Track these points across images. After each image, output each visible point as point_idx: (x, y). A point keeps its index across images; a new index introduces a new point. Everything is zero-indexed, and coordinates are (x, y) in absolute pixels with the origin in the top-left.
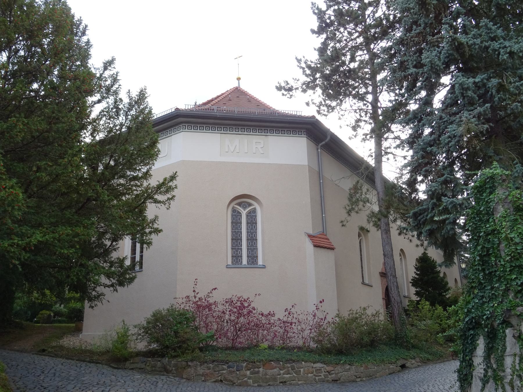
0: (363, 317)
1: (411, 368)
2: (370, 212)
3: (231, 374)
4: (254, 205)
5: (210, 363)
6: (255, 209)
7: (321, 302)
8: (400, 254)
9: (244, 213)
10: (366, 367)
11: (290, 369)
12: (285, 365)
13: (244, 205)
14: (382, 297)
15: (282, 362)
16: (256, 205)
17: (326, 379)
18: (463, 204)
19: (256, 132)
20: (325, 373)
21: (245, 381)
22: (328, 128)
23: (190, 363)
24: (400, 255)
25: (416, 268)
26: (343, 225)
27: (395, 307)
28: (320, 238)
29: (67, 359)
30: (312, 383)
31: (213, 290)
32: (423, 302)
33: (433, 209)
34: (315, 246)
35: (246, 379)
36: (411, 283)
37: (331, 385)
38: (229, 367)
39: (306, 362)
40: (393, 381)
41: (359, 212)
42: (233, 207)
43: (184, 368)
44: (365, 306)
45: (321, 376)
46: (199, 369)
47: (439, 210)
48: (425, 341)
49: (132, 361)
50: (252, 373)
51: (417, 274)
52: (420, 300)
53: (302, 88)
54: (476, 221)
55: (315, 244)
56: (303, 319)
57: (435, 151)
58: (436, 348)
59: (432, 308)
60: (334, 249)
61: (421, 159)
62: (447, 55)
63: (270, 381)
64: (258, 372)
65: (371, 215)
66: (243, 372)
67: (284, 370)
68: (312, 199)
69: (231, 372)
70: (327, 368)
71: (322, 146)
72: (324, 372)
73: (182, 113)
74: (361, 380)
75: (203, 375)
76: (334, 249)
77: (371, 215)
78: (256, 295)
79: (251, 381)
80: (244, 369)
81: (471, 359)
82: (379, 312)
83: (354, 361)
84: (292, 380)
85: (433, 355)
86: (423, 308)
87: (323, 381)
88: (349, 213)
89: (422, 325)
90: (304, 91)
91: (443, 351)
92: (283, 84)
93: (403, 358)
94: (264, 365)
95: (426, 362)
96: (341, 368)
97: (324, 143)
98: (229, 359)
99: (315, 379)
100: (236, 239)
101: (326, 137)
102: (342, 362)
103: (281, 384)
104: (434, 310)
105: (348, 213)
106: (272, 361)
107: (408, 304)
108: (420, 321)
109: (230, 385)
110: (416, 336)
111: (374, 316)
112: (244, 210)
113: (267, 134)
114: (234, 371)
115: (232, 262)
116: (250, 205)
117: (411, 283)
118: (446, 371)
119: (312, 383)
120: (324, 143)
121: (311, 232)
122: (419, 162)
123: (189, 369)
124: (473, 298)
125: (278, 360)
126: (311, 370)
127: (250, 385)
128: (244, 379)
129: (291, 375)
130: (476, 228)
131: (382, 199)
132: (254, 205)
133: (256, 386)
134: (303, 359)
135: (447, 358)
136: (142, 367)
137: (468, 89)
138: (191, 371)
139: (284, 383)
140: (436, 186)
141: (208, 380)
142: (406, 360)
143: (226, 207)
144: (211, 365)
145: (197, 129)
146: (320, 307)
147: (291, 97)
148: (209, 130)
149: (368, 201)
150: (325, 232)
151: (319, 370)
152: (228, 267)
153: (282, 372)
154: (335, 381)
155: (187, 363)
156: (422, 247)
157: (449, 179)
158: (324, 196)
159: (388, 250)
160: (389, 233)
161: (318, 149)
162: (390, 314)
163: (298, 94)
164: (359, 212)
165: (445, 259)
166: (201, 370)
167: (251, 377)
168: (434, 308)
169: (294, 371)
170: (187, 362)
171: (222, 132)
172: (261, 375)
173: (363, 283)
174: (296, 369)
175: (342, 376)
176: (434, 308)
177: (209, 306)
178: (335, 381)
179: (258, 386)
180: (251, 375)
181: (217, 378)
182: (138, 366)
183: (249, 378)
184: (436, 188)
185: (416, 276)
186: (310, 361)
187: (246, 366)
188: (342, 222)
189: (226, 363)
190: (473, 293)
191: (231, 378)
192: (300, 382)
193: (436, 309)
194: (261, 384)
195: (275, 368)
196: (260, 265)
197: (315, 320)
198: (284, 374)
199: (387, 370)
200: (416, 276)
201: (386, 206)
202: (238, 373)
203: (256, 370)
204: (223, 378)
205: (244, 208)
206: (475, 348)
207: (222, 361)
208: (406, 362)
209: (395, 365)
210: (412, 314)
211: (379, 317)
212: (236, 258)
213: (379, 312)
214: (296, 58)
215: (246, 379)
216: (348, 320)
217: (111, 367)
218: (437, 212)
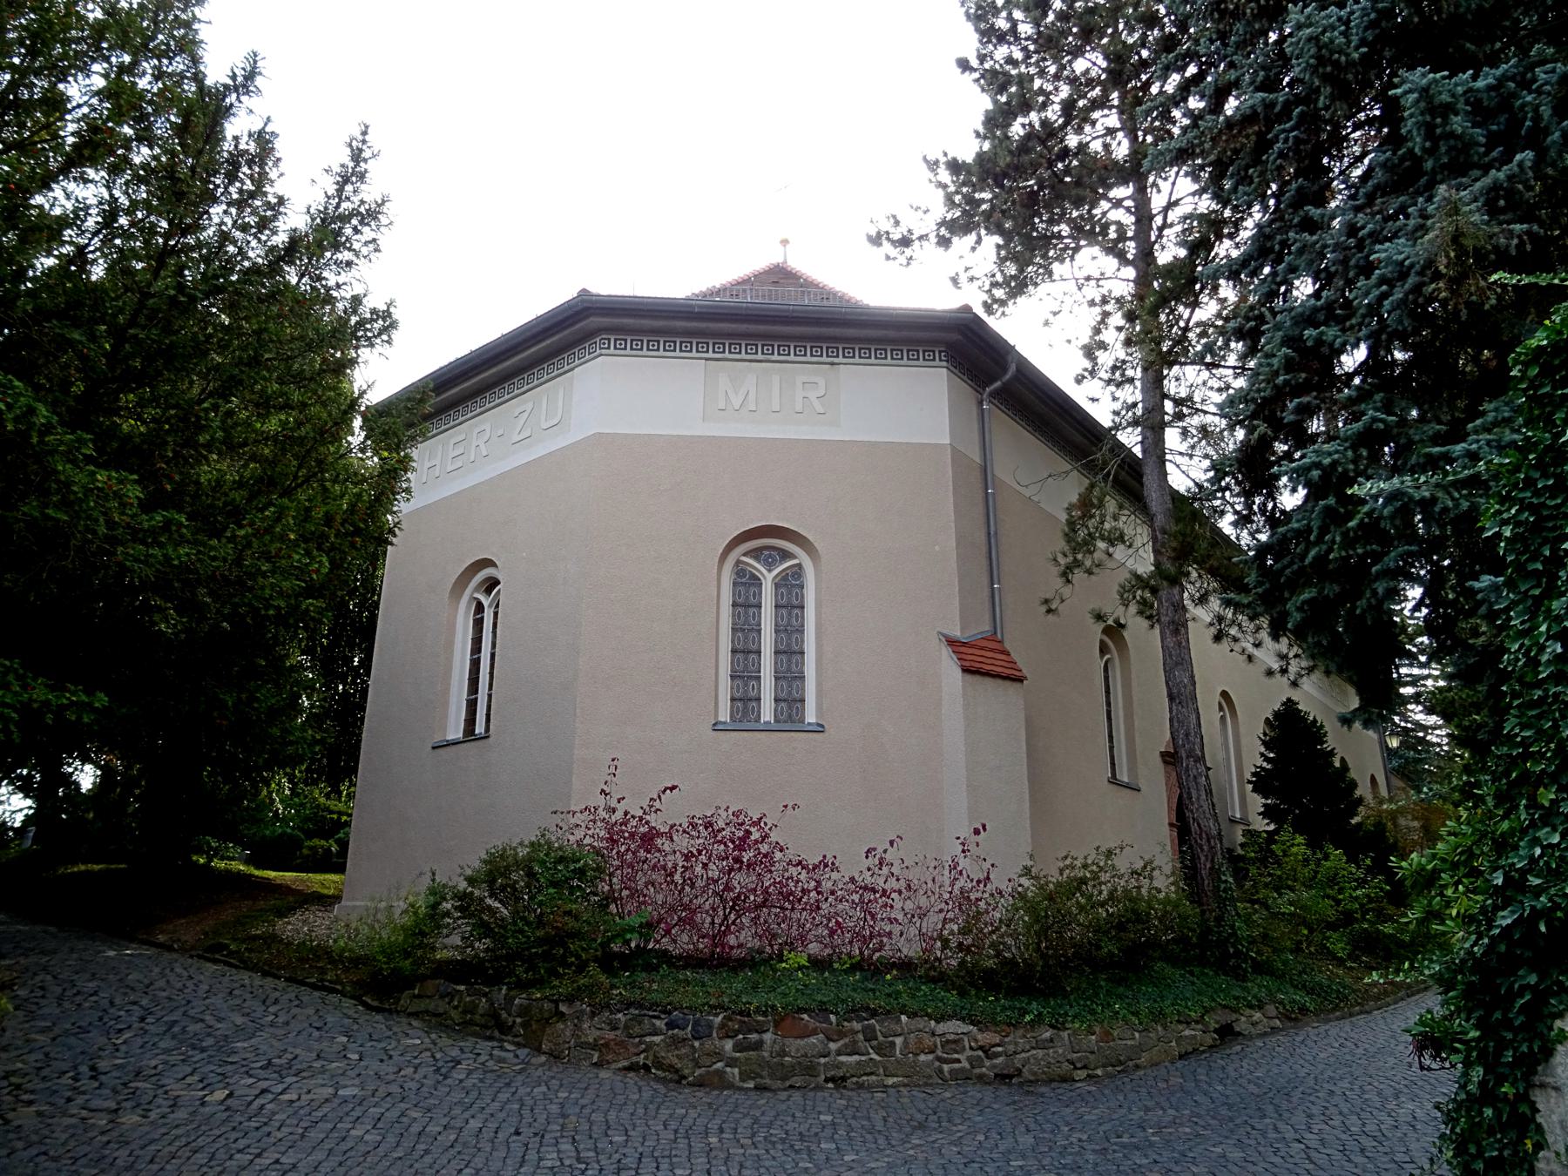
0: (1104, 877)
1: (1251, 1038)
2: (1128, 576)
5: (619, 1011)
6: (799, 566)
7: (977, 832)
8: (1220, 704)
9: (768, 578)
10: (1108, 1034)
11: (861, 1036)
12: (846, 1024)
13: (770, 556)
14: (1167, 821)
15: (836, 1014)
16: (802, 557)
17: (977, 1071)
18: (1433, 500)
19: (805, 355)
20: (971, 1053)
21: (717, 1071)
22: (1012, 343)
24: (1221, 708)
25: (1264, 743)
26: (1049, 611)
27: (1202, 850)
28: (982, 648)
29: (265, 974)
30: (931, 1085)
31: (664, 792)
32: (1284, 836)
33: (1324, 531)
34: (966, 670)
36: (1249, 782)
37: (988, 1093)
39: (912, 1015)
40: (1190, 1085)
41: (1095, 570)
42: (738, 562)
43: (547, 1020)
44: (1112, 845)
45: (958, 1061)
47: (1348, 530)
48: (1292, 952)
49: (416, 992)
50: (738, 1047)
51: (1267, 759)
52: (1276, 832)
53: (938, 235)
54: (1537, 493)
55: (967, 664)
56: (923, 880)
57: (1331, 338)
58: (1325, 974)
59: (1314, 853)
60: (1022, 681)
61: (1281, 372)
62: (1373, 16)
63: (795, 1075)
64: (758, 1045)
65: (1133, 583)
66: (714, 1042)
67: (841, 1042)
68: (960, 540)
69: (676, 1042)
70: (979, 1037)
71: (993, 395)
72: (971, 1048)
74: (1088, 1076)
75: (594, 1046)
76: (1022, 681)
77: (1133, 583)
78: (786, 806)
79: (736, 1071)
80: (715, 1035)
81: (1524, 1097)
82: (1151, 862)
83: (1066, 1014)
84: (866, 1074)
85: (1319, 995)
86: (1285, 854)
87: (962, 1077)
88: (1066, 575)
89: (1284, 904)
90: (944, 242)
91: (1348, 980)
92: (886, 226)
93: (1225, 1007)
94: (777, 1025)
95: (1294, 1017)
96: (1025, 1036)
97: (998, 384)
98: (676, 998)
99: (941, 1071)
100: (745, 652)
101: (1005, 370)
102: (1028, 1018)
103: (830, 1085)
104: (1319, 860)
105: (1064, 574)
106: (805, 1011)
107: (1241, 839)
108: (1277, 889)
109: (671, 1081)
110: (1265, 936)
111: (1140, 875)
112: (770, 571)
113: (836, 360)
114: (684, 1040)
115: (731, 717)
116: (786, 555)
117: (1249, 782)
118: (1360, 1051)
119: (931, 1085)
120: (998, 384)
121: (956, 633)
122: (1276, 386)
123: (561, 1026)
124: (1533, 824)
125: (823, 1010)
126: (928, 1041)
127: (731, 1086)
128: (715, 1067)
129: (863, 1058)
130: (1536, 528)
131: (1164, 532)
132: (795, 557)
133: (750, 1089)
134: (905, 1006)
135: (1359, 1004)
136: (441, 1010)
137: (1448, 110)
138: (564, 1029)
139: (839, 1081)
140: (1337, 452)
141: (608, 1063)
142: (1236, 1010)
143: (717, 560)
144: (620, 1015)
145: (641, 349)
146: (972, 847)
147: (908, 264)
148: (675, 350)
149: (1121, 538)
150: (999, 636)
151: (954, 1044)
152: (717, 727)
153: (833, 1046)
154: (1003, 1078)
155: (557, 1007)
156: (1285, 679)
157: (1381, 426)
158: (996, 533)
159: (1182, 681)
160: (1183, 631)
161: (981, 403)
162: (1190, 871)
163: (927, 252)
164: (1095, 570)
165: (1361, 700)
166: (592, 1031)
167: (737, 1059)
168: (1319, 856)
169: (874, 1043)
170: (556, 1002)
172: (766, 1054)
173: (1114, 780)
174: (881, 1038)
175: (1026, 1062)
176: (1319, 856)
177: (648, 839)
178: (1003, 1078)
179: (756, 1088)
181: (634, 1059)
182: (431, 1005)
183: (731, 1063)
184: (1336, 456)
185: (1265, 764)
186: (927, 1015)
187: (722, 1026)
188: (1046, 601)
189: (664, 1012)
190: (1533, 804)
192: (890, 1081)
193: (1326, 858)
194: (768, 1081)
195: (814, 1032)
196: (809, 724)
197: (958, 885)
198: (839, 1053)
199: (1173, 1044)
200: (1265, 764)
201: (1174, 550)
202: (697, 1044)
203: (754, 1036)
204: (651, 1058)
205: (770, 567)
206: (1548, 1052)
207: (653, 1005)
208: (1234, 1016)
209: (1200, 1026)
210: (1253, 871)
211: (1151, 878)
212: (745, 702)
213: (1151, 862)
214: (925, 158)
215: (719, 1065)
216: (1059, 884)
217: (365, 1004)
218: (1338, 539)
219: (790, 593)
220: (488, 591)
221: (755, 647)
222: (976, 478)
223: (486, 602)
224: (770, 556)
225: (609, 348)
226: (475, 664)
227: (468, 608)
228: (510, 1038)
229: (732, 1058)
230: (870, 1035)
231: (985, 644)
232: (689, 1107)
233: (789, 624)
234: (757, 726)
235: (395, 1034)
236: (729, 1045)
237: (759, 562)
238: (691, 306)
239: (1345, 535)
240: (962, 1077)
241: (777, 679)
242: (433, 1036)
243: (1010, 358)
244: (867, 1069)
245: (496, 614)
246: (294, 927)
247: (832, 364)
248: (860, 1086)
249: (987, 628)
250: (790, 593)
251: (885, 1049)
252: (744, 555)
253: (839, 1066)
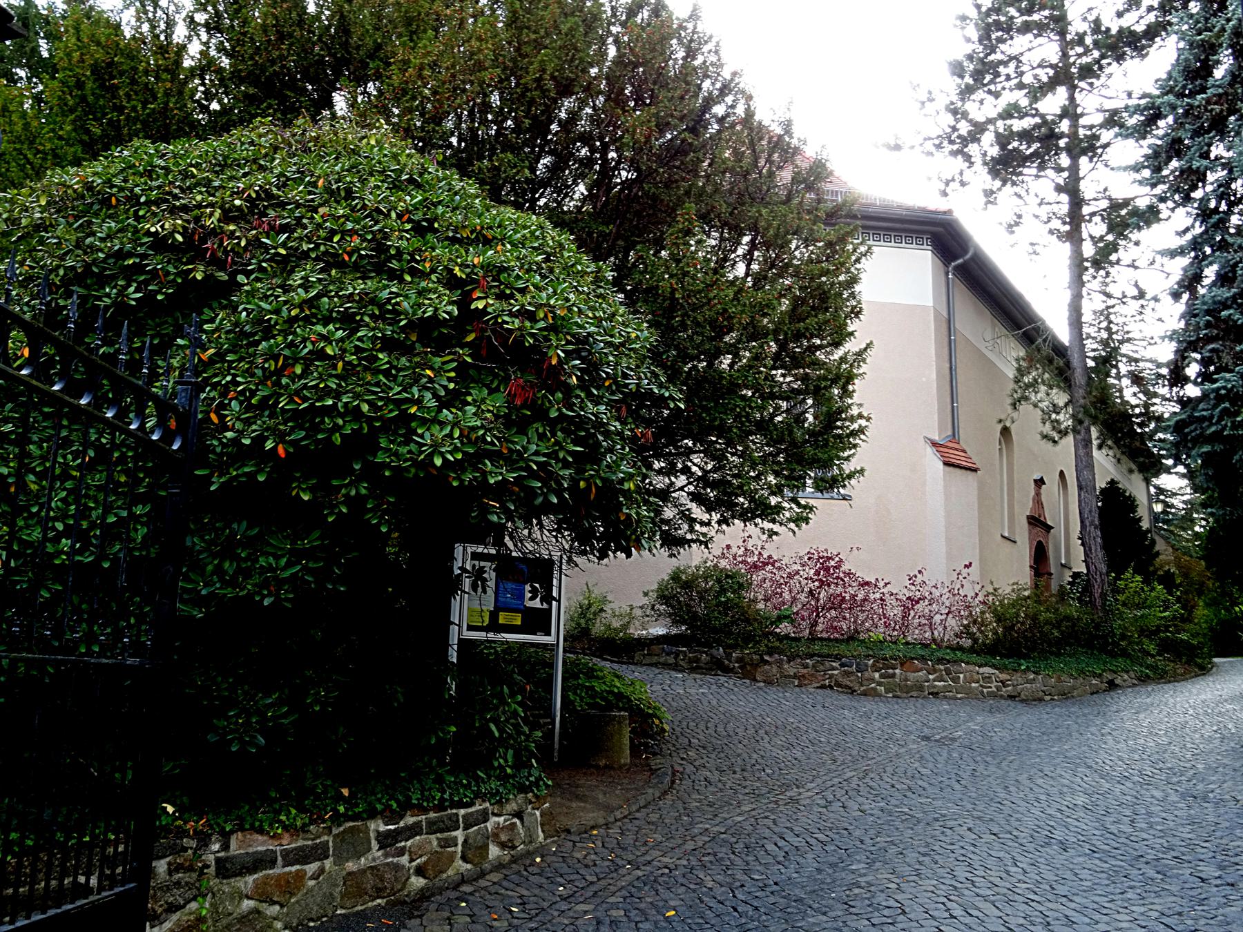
23: (767, 658)
33: (1220, 419)
34: (946, 464)
38: (842, 665)
39: (967, 663)
46: (786, 666)
50: (882, 676)
69: (847, 674)
75: (795, 677)
87: (993, 695)
88: (1014, 406)
94: (902, 665)
95: (1144, 680)
97: (960, 261)
101: (966, 252)
120: (960, 261)
121: (936, 438)
126: (976, 677)
127: (880, 696)
139: (935, 694)
142: (1115, 672)
151: (987, 679)
153: (931, 677)
161: (947, 274)
166: (790, 669)
178: (1011, 697)
183: (879, 684)
187: (873, 665)
195: (921, 670)
198: (934, 680)
222: (945, 326)
230: (948, 672)
232: (867, 705)
236: (877, 675)
239: (1233, 423)
240: (993, 695)
244: (947, 689)
248: (945, 697)
251: (956, 680)
253: (935, 687)
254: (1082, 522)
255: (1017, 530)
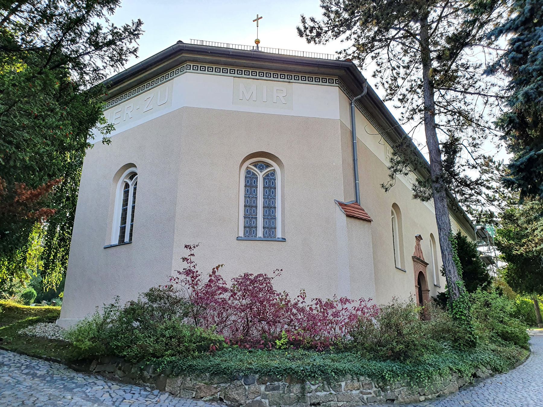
3: (237, 390)
4: (272, 166)
6: (274, 170)
9: (261, 175)
16: (275, 166)
28: (353, 207)
34: (348, 216)
35: (258, 398)
42: (248, 167)
71: (355, 100)
73: (186, 47)
79: (267, 401)
88: (392, 176)
112: (261, 172)
113: (291, 81)
115: (263, 235)
116: (268, 165)
120: (360, 96)
121: (342, 200)
132: (272, 166)
150: (358, 202)
152: (238, 239)
161: (351, 104)
171: (236, 75)
180: (267, 393)
183: (265, 397)
191: (236, 397)
196: (278, 238)
198: (316, 390)
205: (261, 169)
219: (270, 182)
220: (131, 178)
221: (254, 205)
223: (130, 183)
224: (261, 165)
225: (190, 69)
226: (125, 211)
227: (121, 186)
228: (148, 384)
229: (264, 394)
231: (353, 205)
233: (269, 195)
234: (274, 239)
235: (89, 383)
237: (257, 168)
238: (229, 51)
241: (264, 218)
242: (110, 384)
243: (364, 85)
245: (135, 189)
246: (40, 330)
247: (289, 82)
249: (353, 200)
250: (270, 182)
252: (250, 164)
254: (442, 252)
255: (406, 264)
